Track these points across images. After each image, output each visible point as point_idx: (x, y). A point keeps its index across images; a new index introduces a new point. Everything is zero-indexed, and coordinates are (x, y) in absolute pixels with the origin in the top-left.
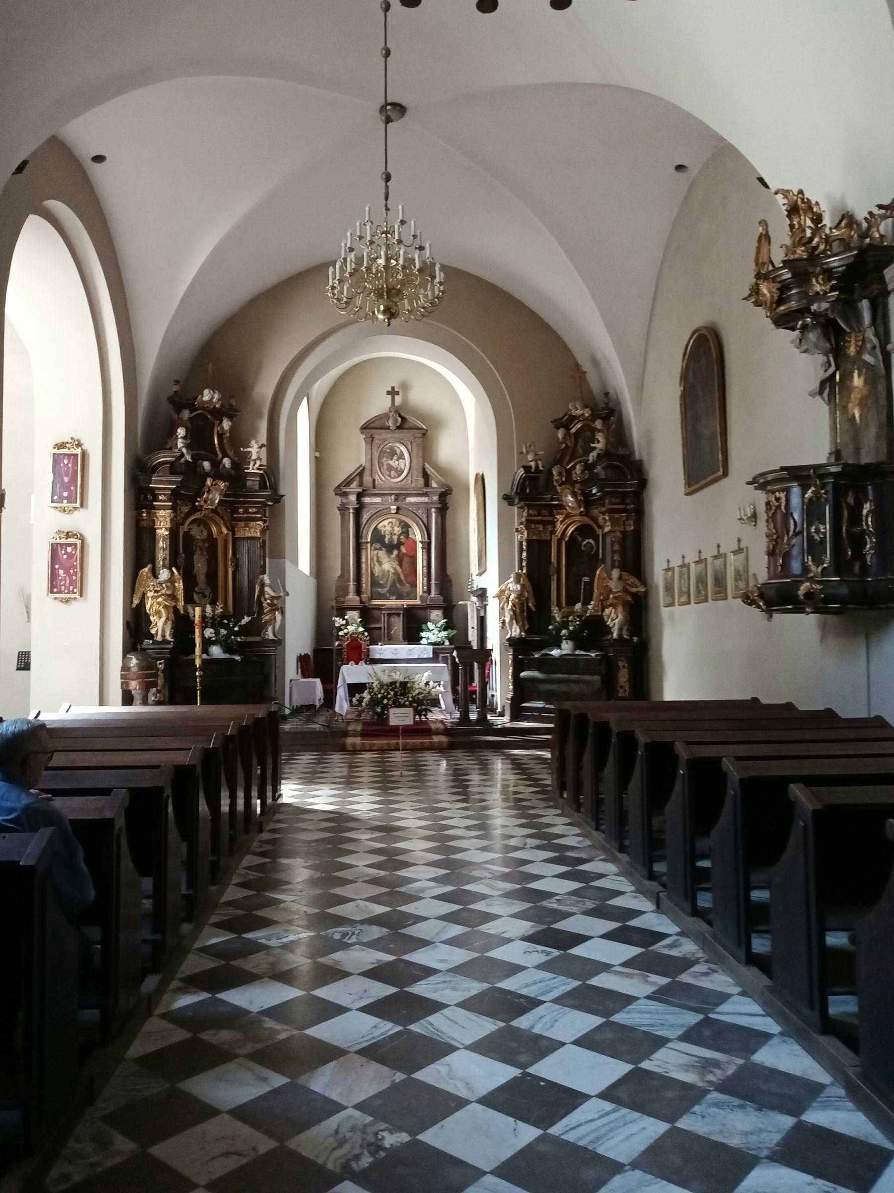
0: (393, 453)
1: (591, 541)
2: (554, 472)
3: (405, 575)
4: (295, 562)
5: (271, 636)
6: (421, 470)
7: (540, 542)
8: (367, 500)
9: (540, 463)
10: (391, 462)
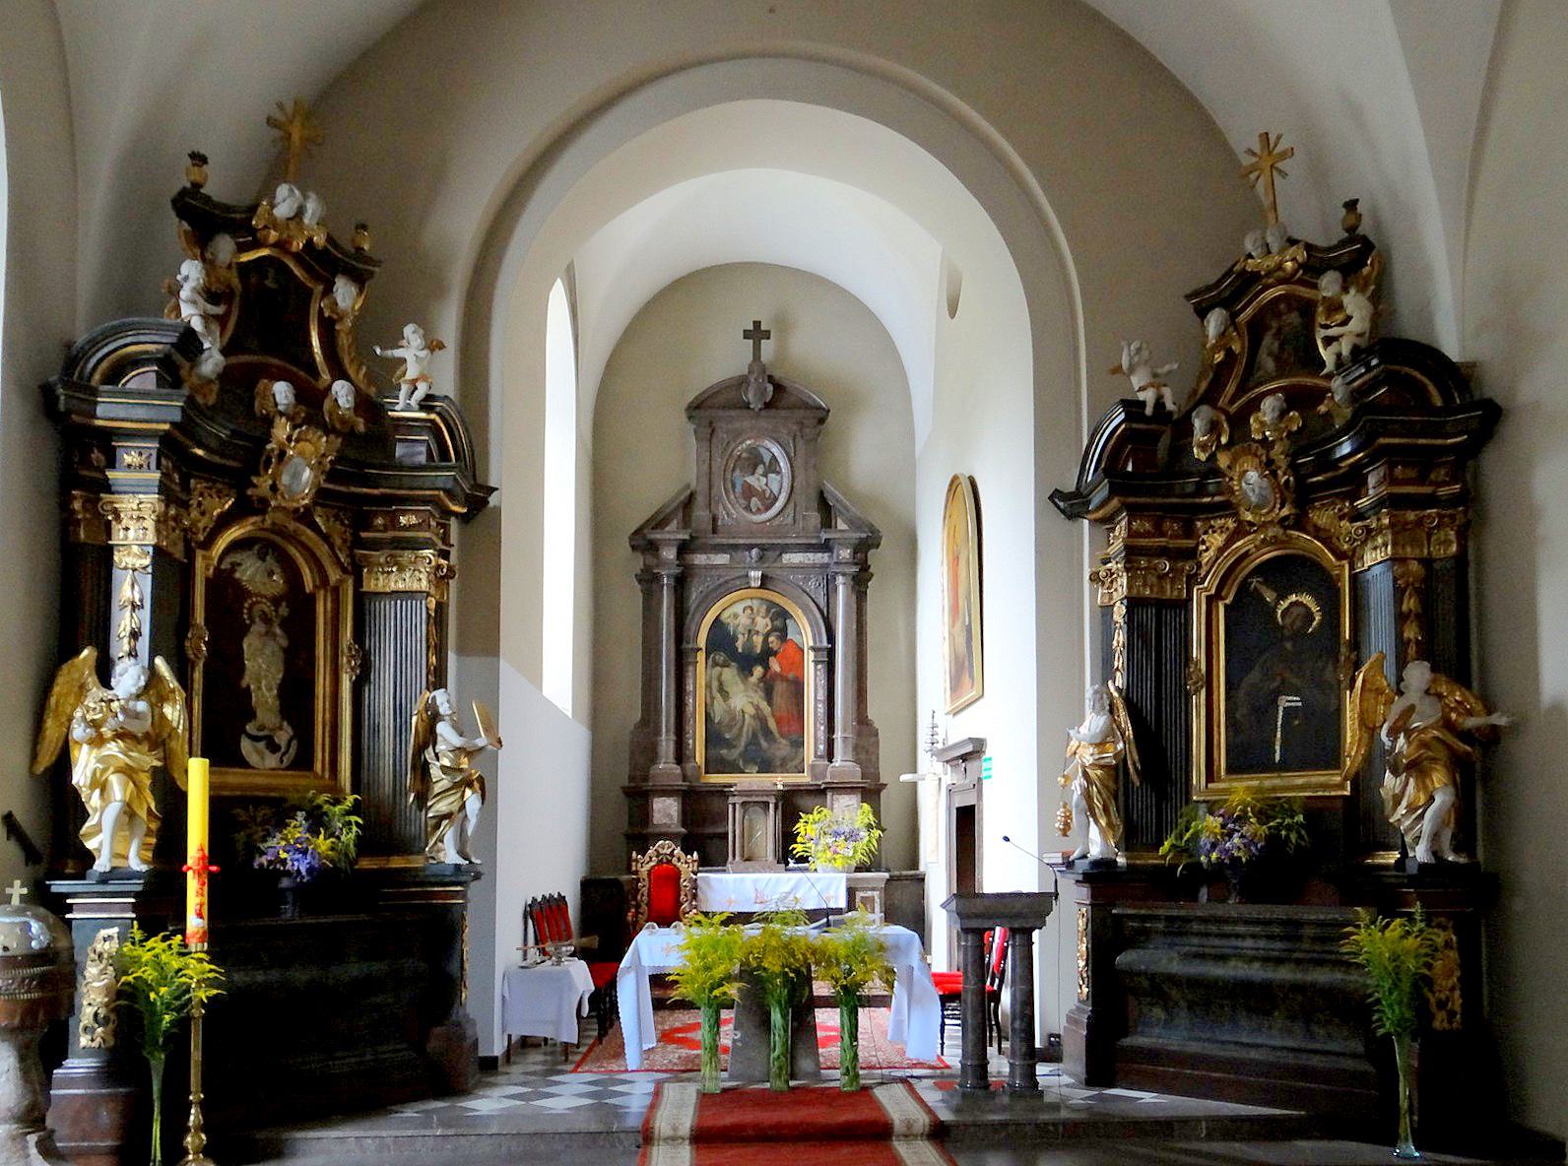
0: (754, 461)
1: (1307, 599)
2: (1197, 423)
3: (779, 722)
4: (536, 678)
5: (450, 856)
6: (813, 494)
7: (1161, 605)
8: (700, 559)
9: (1167, 392)
10: (750, 480)
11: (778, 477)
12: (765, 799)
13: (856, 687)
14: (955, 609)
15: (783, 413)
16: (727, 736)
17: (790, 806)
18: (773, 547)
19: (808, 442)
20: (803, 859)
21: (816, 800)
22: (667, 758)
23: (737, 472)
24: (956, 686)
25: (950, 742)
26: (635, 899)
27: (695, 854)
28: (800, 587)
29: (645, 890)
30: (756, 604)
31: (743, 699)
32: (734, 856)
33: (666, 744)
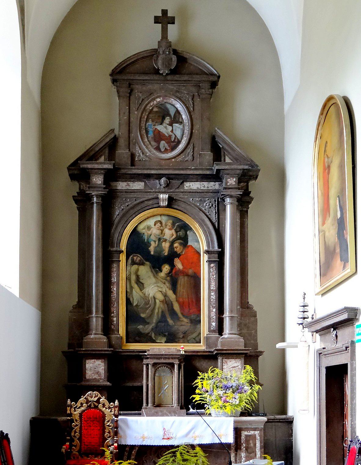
0: (162, 114)
3: (182, 305)
6: (208, 141)
8: (122, 185)
10: (160, 128)
11: (181, 127)
12: (171, 361)
13: (239, 280)
14: (325, 210)
15: (186, 78)
16: (143, 315)
17: (191, 368)
19: (203, 100)
20: (201, 406)
21: (209, 363)
22: (96, 329)
23: (150, 122)
24: (325, 269)
25: (319, 316)
26: (70, 435)
27: (117, 402)
28: (197, 207)
29: (77, 429)
30: (164, 219)
31: (155, 288)
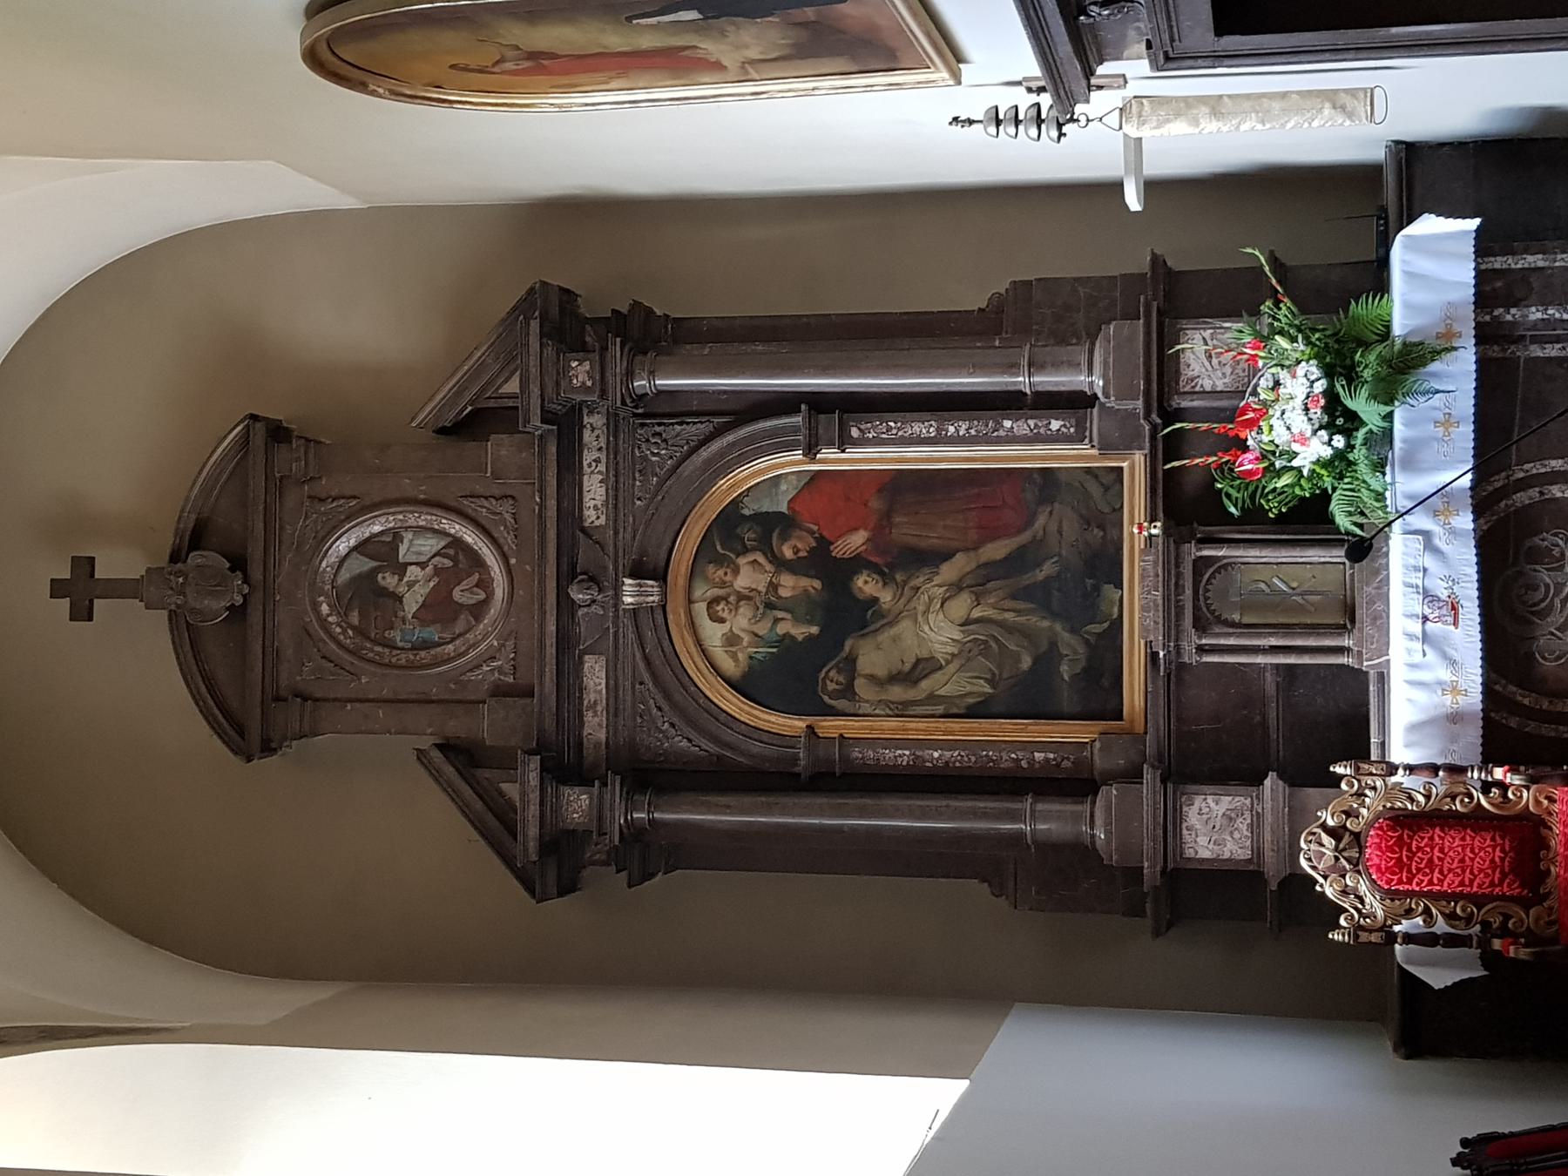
0: (368, 597)
3: (991, 533)
8: (595, 727)
10: (412, 604)
11: (408, 536)
12: (1188, 570)
16: (1026, 662)
18: (567, 552)
23: (396, 635)
25: (1031, 67)
27: (1339, 769)
28: (661, 484)
31: (934, 624)
32: (1340, 650)
33: (1045, 821)
